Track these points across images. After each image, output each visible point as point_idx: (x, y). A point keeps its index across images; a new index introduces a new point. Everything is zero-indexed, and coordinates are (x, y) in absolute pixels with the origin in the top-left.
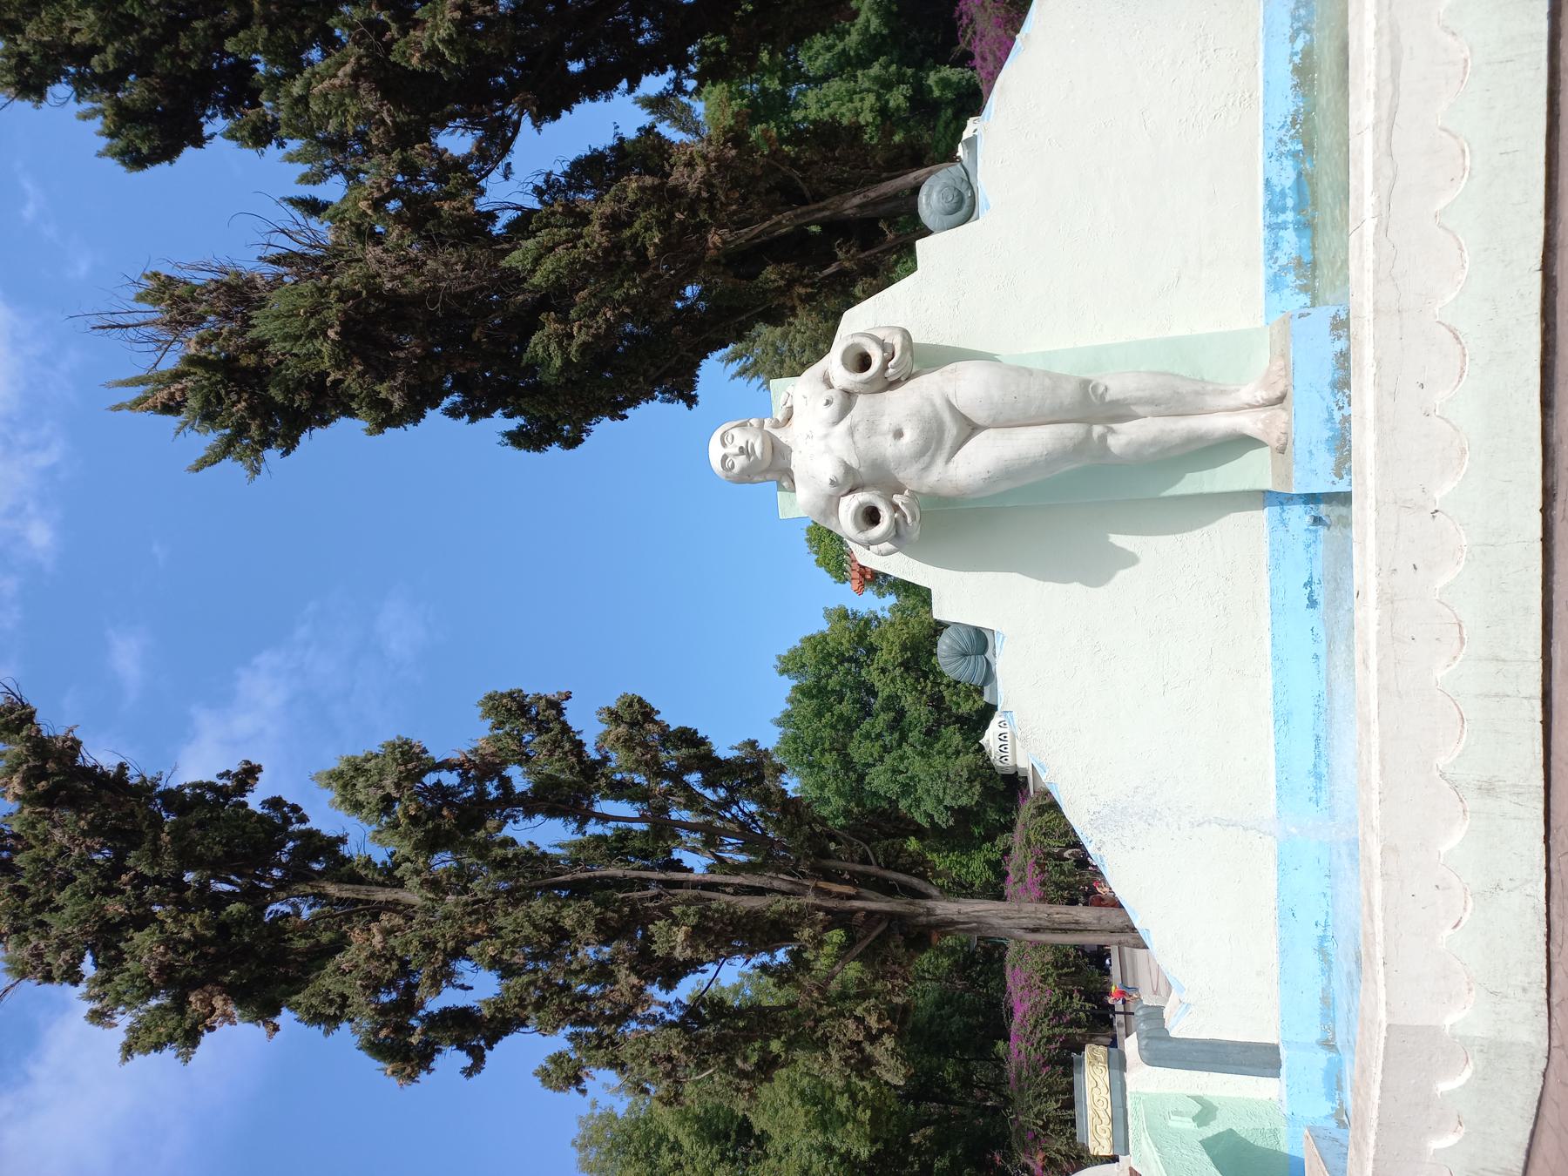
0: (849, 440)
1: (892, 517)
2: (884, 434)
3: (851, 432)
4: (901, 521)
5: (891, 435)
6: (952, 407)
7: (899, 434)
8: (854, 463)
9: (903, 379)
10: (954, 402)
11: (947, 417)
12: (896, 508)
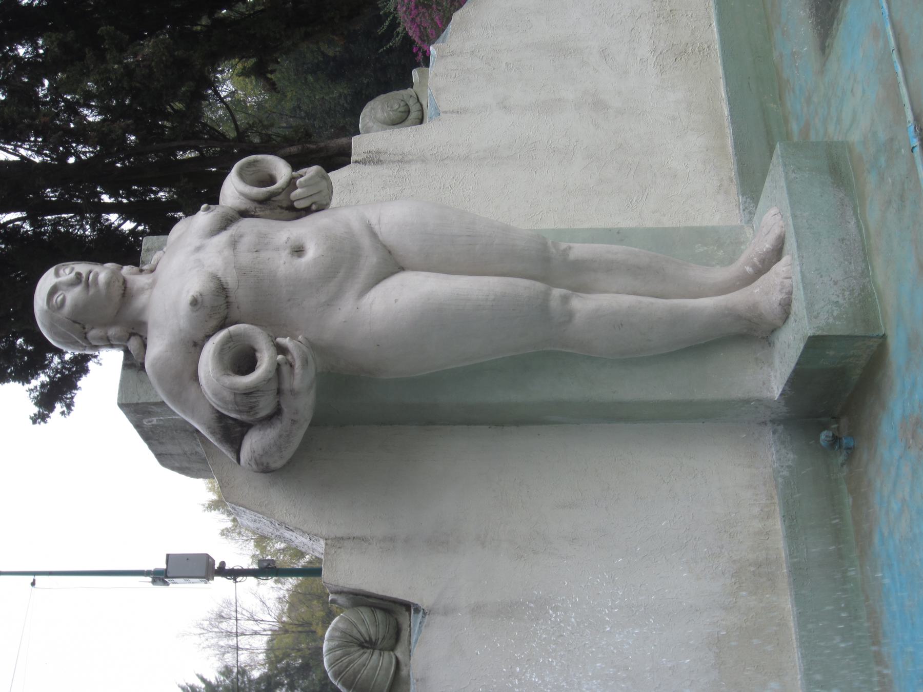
0: (227, 253)
1: (271, 358)
2: (277, 249)
3: (234, 243)
4: (285, 369)
5: (288, 251)
6: (373, 234)
7: (298, 251)
8: (230, 280)
9: (314, 207)
10: (376, 228)
11: (366, 242)
12: (281, 350)
